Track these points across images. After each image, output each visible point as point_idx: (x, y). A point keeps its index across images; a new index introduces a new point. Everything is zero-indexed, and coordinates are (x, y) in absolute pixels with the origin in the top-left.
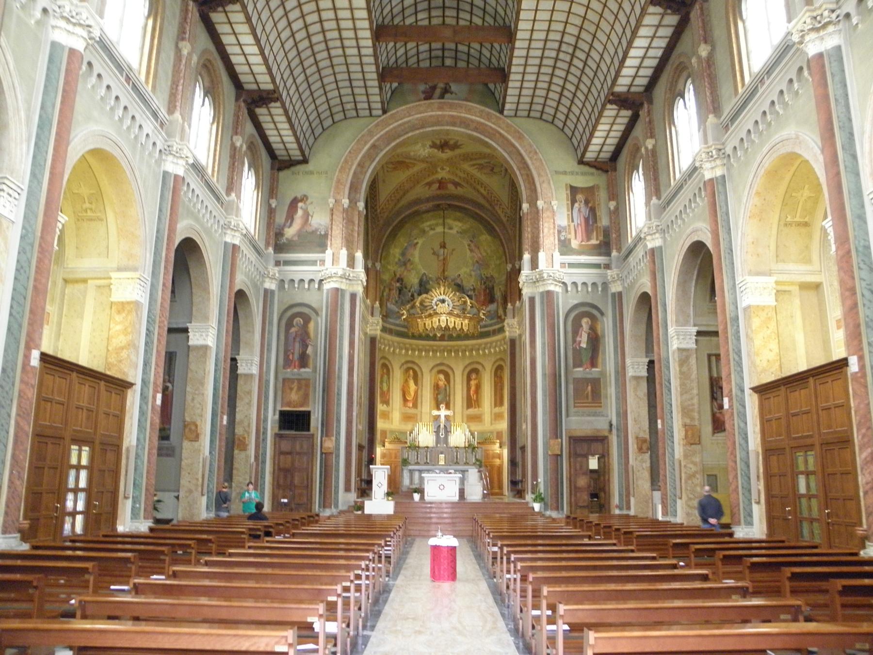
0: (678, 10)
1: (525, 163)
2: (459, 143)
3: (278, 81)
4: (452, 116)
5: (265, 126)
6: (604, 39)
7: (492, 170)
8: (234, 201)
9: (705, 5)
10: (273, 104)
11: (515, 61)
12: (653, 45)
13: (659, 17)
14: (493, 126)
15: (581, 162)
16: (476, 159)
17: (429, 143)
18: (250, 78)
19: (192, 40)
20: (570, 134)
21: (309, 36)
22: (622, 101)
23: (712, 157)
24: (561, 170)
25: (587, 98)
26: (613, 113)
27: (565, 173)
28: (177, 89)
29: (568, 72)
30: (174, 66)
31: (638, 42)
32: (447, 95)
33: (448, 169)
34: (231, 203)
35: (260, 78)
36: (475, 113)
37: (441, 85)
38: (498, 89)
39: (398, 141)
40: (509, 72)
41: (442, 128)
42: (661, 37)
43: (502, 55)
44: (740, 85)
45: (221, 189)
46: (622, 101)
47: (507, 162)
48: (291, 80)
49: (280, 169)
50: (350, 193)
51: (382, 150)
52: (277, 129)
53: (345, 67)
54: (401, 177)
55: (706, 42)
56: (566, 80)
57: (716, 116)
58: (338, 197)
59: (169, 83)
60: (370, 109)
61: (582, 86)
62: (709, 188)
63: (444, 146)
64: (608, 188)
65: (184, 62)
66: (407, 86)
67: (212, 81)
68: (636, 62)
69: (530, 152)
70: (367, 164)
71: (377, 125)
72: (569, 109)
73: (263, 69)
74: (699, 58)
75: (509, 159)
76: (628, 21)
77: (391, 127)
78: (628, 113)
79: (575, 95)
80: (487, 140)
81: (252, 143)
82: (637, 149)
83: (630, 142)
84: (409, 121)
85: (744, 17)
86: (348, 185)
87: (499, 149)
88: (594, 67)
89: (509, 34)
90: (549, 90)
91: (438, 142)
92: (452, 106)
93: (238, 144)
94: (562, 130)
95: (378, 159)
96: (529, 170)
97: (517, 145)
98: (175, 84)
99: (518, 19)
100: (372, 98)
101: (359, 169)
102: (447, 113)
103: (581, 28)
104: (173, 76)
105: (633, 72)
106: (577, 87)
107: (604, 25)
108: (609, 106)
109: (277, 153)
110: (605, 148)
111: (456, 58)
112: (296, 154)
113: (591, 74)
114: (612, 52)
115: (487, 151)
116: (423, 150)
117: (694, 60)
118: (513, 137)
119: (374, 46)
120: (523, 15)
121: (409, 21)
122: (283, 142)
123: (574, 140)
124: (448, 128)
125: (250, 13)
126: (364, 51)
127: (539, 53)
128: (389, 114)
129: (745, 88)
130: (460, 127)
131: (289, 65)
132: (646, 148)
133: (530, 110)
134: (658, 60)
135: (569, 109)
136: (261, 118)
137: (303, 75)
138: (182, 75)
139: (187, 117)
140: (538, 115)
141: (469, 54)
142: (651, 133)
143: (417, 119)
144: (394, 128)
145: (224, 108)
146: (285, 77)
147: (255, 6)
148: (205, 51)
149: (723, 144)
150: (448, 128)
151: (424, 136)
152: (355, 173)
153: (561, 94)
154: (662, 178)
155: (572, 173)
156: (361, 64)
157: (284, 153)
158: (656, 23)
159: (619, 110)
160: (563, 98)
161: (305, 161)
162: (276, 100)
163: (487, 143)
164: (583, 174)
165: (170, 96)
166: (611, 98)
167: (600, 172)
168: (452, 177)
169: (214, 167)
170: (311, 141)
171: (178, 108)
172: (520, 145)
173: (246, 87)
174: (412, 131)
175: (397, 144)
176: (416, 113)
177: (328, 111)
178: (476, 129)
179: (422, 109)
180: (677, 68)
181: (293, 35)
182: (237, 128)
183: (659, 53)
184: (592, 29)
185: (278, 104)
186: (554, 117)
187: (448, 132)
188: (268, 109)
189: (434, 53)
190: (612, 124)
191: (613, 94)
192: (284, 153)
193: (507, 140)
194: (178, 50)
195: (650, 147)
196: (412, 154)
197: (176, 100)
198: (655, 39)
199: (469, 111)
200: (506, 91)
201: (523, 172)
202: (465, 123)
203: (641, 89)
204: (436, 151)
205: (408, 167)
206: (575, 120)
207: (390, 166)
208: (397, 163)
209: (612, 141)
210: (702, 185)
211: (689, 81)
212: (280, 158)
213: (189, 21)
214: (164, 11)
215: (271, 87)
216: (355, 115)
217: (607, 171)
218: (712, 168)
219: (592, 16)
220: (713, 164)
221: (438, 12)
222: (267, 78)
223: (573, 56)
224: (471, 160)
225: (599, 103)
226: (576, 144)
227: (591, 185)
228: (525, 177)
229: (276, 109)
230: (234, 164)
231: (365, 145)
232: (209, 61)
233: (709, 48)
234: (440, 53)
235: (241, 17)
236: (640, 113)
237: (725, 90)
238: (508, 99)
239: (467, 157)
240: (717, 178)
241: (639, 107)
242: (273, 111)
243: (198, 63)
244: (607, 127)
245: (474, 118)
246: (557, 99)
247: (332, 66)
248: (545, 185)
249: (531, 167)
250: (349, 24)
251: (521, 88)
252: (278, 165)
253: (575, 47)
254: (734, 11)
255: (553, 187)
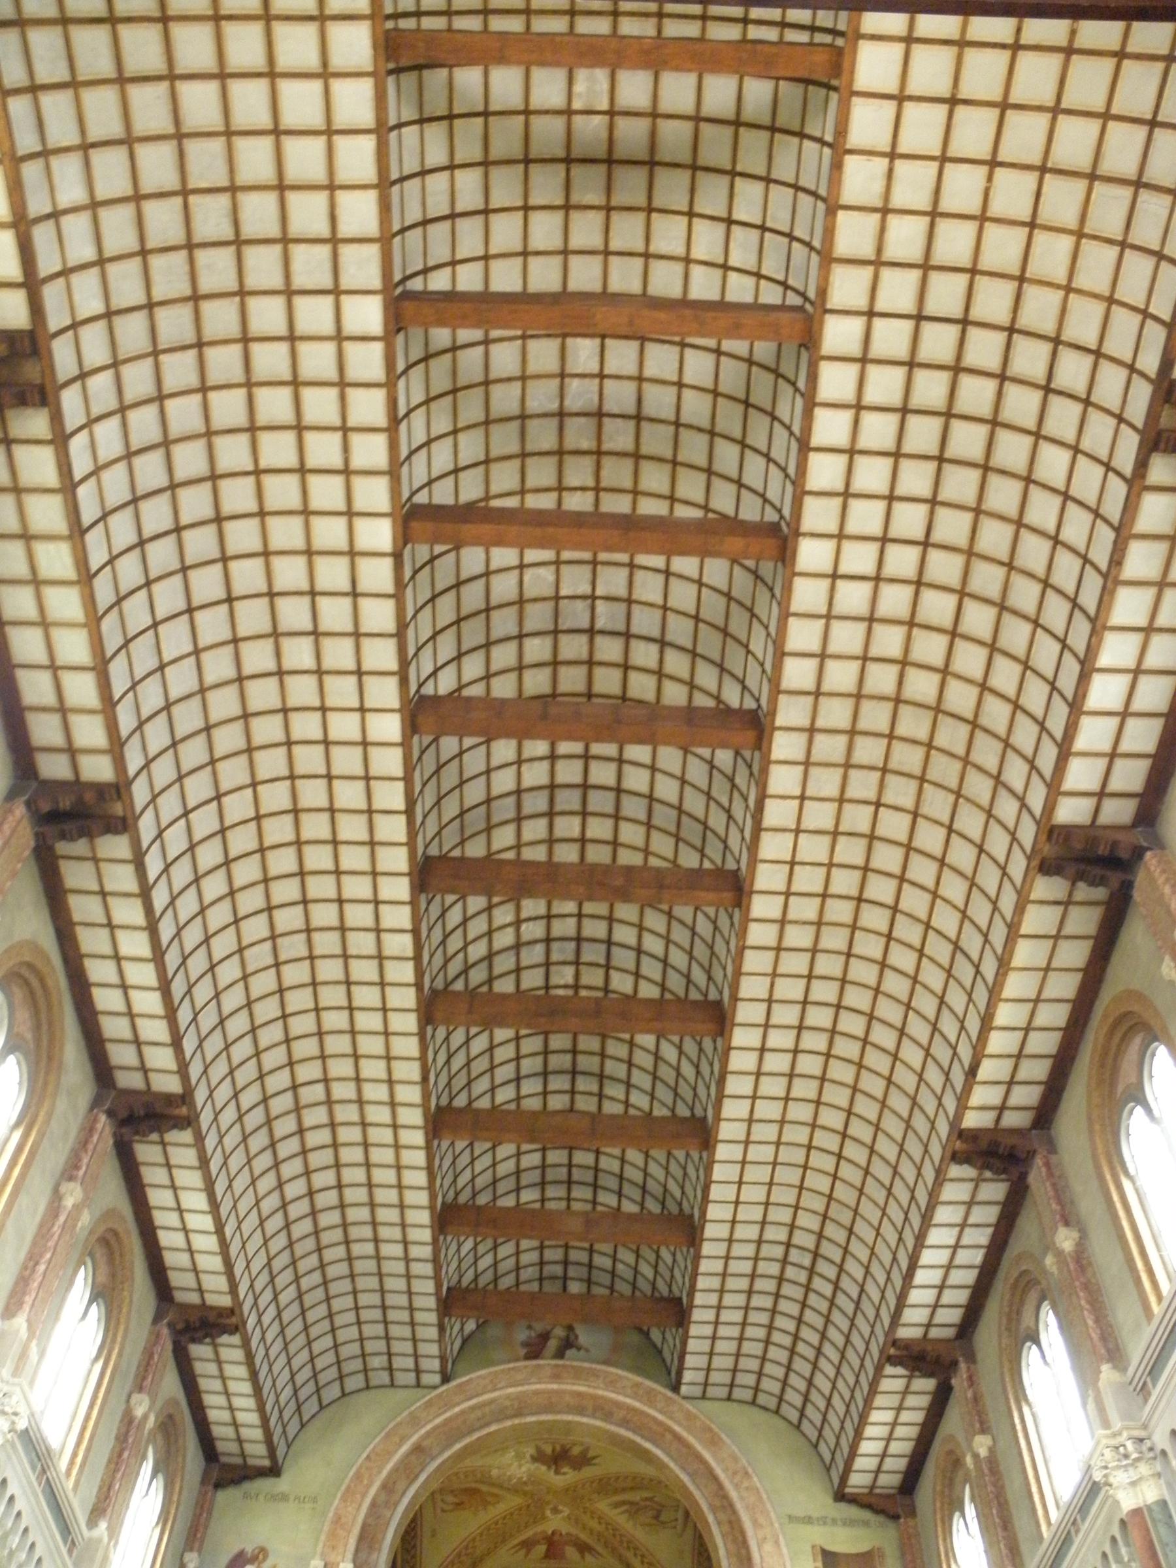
0: (1004, 1171)
1: (725, 1497)
2: (591, 1454)
3: (242, 1290)
4: (580, 1395)
5: (203, 1384)
6: (869, 1235)
7: (657, 1517)
8: (100, 1540)
9: (1054, 1159)
10: (225, 1339)
11: (701, 1283)
12: (965, 1241)
13: (970, 1186)
14: (660, 1417)
15: (841, 1496)
16: (624, 1490)
17: (530, 1451)
18: (188, 1280)
19: (90, 1185)
20: (813, 1434)
21: (314, 1213)
22: (917, 1358)
23: (1126, 1456)
24: (800, 1512)
25: (843, 1356)
26: (899, 1384)
27: (808, 1520)
28: (33, 1271)
29: (804, 1305)
30: (41, 1226)
31: (935, 1236)
32: (570, 1353)
33: (566, 1512)
34: (93, 1544)
35: (209, 1282)
36: (625, 1388)
37: (559, 1332)
38: (672, 1337)
39: (467, 1440)
40: (691, 1306)
41: (559, 1417)
42: (1042, 902)
43: (677, 1273)
44: (1152, 1299)
45: (78, 1506)
46: (917, 1358)
47: (689, 1495)
48: (268, 1295)
49: (218, 1486)
50: (357, 1551)
51: (433, 1459)
52: (227, 1393)
53: (376, 1279)
54: (465, 1527)
55: (1067, 1224)
56: (800, 1321)
57: (1115, 1367)
58: (333, 1558)
59: (23, 1255)
60: (418, 1371)
61: (832, 1333)
62: (1135, 1534)
63: (559, 1458)
64: (903, 1555)
65: (62, 1219)
66: (494, 1331)
67: (113, 1275)
68: (935, 1277)
69: (735, 1473)
70: (400, 1486)
71: (429, 1404)
72: (810, 1382)
73: (216, 1263)
74: (1059, 1254)
75: (692, 1487)
76: (913, 1198)
77: (457, 1409)
78: (928, 1384)
79: (819, 1351)
80: (648, 1445)
81: (170, 1417)
82: (957, 1462)
83: (937, 1449)
84: (492, 1401)
85: (1132, 1171)
86: (356, 1531)
87: (672, 1465)
88: (854, 1292)
89: (689, 1230)
90: (767, 1342)
91: (548, 1449)
92: (578, 1375)
93: (139, 1412)
94: (798, 1427)
95: (422, 1478)
96: (734, 1512)
97: (707, 1456)
98: (33, 1259)
99: (705, 1199)
100: (423, 1348)
101: (383, 1497)
102: (569, 1387)
103: (825, 1217)
104: (34, 1244)
105: (932, 1295)
106: (823, 1336)
107: (866, 1208)
108: (889, 1370)
109: (221, 1446)
110: (889, 1464)
111: (589, 1281)
112: (257, 1452)
113: (840, 1340)
114: (887, 1258)
115: (649, 1471)
116: (516, 1466)
117: (1049, 1260)
118: (700, 1441)
119: (435, 1242)
120: (715, 1192)
121: (509, 1202)
122: (235, 1424)
123: (823, 1447)
124: (570, 1418)
125: (188, 1055)
126: (415, 1252)
127: (746, 1267)
128: (453, 1383)
129: (1165, 1303)
130: (593, 1416)
131: (282, 1331)
132: (976, 1456)
133: (732, 1385)
134: (976, 1272)
135: (810, 1382)
136: (199, 1367)
137: (293, 1287)
138: (51, 1244)
139: (39, 1329)
140: (747, 1395)
141: (613, 1273)
142: (982, 1423)
143: (508, 1397)
144: (463, 1412)
145: (125, 1337)
146: (258, 1286)
147: (220, 1142)
148: (110, 1214)
149: (1145, 1427)
150: (570, 1418)
151: (519, 1436)
152: (373, 1504)
153: (792, 1352)
154: (1021, 1523)
155: (823, 1521)
156: (414, 1340)
157: (233, 1447)
158: (966, 1197)
159: (910, 1378)
160: (796, 1358)
161: (274, 1471)
162: (234, 1330)
163: (647, 1452)
164: (849, 1523)
165: (16, 1284)
166: (892, 1351)
167: (881, 1518)
168: (574, 1531)
169: (75, 1454)
170: (292, 1429)
171: (27, 1307)
172: (714, 1456)
173: (180, 1297)
174: (498, 1421)
175: (465, 1448)
176: (510, 1385)
177: (334, 1369)
178: (625, 1423)
179: (519, 1377)
180: (1015, 1286)
181: (284, 1206)
182: (144, 1378)
183: (978, 1257)
184: (846, 1217)
185: (236, 1339)
186: (781, 1399)
187: (568, 1427)
188: (215, 1346)
189: (549, 1270)
190: (899, 1409)
191: (895, 1343)
192: (233, 1447)
193: (688, 1446)
194: (57, 1195)
195: (983, 1452)
196: (495, 1472)
197: (30, 1289)
198: (967, 1230)
199: (612, 1384)
200: (684, 1343)
201: (722, 1516)
202: (603, 1409)
203: (950, 1333)
204: (544, 1468)
205: (485, 1504)
206: (822, 1404)
207: (450, 1499)
208: (463, 1491)
209: (902, 1447)
210: (1116, 1531)
211: (1046, 1308)
212: (224, 1459)
213: (90, 1147)
214: (48, 1121)
215: (226, 1301)
216: (387, 1381)
217: (895, 1517)
218: (1133, 1484)
219: (844, 1193)
220: (1133, 1474)
221: (561, 1191)
222: (222, 1283)
223: (812, 1271)
224: (616, 1491)
225: (868, 1364)
226: (827, 1457)
227: (863, 1547)
228: (726, 1528)
229: (230, 1349)
230: (120, 1455)
231: (400, 1445)
232: (116, 1233)
233: (1075, 1235)
234: (558, 1270)
235: (188, 1156)
236: (953, 1382)
237: (1124, 1313)
238: (690, 1361)
239: (605, 1486)
240: (1148, 1507)
241: (952, 1365)
242: (225, 1353)
243: (91, 1232)
244: (888, 1416)
245: (621, 1398)
246: (785, 1361)
247: (352, 1276)
248: (768, 1547)
249: (739, 1506)
250: (388, 1156)
251: (714, 1338)
252: (218, 1472)
253: (816, 1255)
254: (1113, 1169)
255: (785, 1550)
